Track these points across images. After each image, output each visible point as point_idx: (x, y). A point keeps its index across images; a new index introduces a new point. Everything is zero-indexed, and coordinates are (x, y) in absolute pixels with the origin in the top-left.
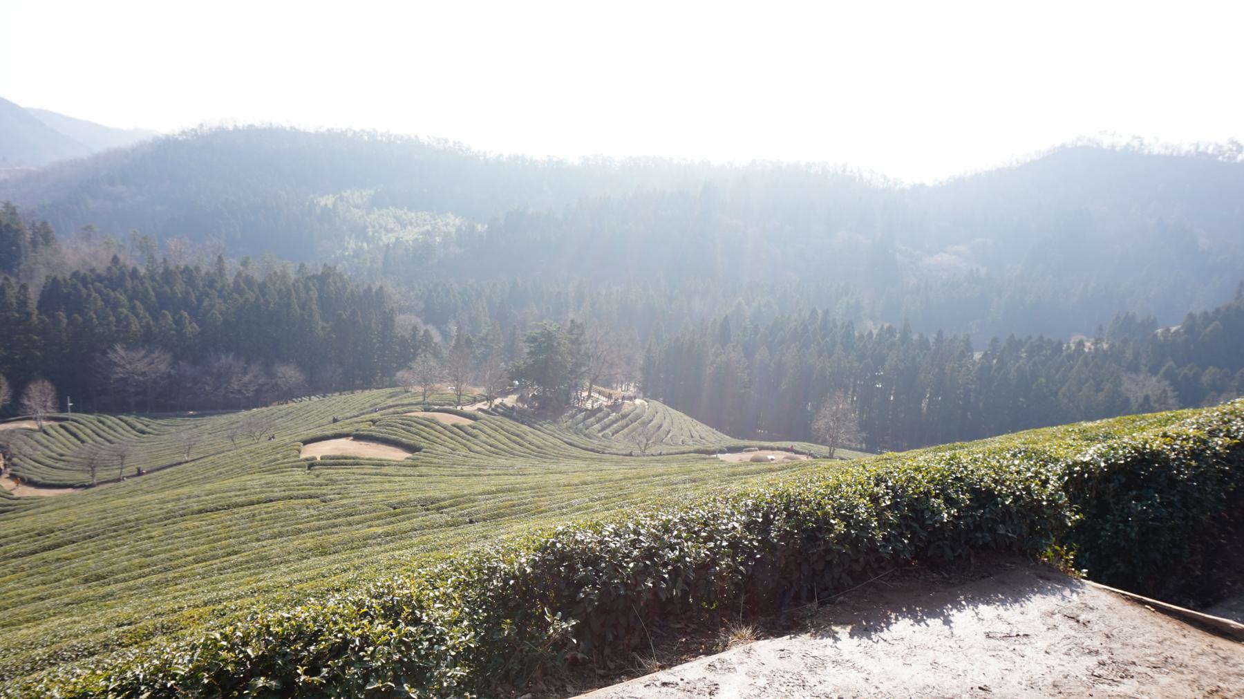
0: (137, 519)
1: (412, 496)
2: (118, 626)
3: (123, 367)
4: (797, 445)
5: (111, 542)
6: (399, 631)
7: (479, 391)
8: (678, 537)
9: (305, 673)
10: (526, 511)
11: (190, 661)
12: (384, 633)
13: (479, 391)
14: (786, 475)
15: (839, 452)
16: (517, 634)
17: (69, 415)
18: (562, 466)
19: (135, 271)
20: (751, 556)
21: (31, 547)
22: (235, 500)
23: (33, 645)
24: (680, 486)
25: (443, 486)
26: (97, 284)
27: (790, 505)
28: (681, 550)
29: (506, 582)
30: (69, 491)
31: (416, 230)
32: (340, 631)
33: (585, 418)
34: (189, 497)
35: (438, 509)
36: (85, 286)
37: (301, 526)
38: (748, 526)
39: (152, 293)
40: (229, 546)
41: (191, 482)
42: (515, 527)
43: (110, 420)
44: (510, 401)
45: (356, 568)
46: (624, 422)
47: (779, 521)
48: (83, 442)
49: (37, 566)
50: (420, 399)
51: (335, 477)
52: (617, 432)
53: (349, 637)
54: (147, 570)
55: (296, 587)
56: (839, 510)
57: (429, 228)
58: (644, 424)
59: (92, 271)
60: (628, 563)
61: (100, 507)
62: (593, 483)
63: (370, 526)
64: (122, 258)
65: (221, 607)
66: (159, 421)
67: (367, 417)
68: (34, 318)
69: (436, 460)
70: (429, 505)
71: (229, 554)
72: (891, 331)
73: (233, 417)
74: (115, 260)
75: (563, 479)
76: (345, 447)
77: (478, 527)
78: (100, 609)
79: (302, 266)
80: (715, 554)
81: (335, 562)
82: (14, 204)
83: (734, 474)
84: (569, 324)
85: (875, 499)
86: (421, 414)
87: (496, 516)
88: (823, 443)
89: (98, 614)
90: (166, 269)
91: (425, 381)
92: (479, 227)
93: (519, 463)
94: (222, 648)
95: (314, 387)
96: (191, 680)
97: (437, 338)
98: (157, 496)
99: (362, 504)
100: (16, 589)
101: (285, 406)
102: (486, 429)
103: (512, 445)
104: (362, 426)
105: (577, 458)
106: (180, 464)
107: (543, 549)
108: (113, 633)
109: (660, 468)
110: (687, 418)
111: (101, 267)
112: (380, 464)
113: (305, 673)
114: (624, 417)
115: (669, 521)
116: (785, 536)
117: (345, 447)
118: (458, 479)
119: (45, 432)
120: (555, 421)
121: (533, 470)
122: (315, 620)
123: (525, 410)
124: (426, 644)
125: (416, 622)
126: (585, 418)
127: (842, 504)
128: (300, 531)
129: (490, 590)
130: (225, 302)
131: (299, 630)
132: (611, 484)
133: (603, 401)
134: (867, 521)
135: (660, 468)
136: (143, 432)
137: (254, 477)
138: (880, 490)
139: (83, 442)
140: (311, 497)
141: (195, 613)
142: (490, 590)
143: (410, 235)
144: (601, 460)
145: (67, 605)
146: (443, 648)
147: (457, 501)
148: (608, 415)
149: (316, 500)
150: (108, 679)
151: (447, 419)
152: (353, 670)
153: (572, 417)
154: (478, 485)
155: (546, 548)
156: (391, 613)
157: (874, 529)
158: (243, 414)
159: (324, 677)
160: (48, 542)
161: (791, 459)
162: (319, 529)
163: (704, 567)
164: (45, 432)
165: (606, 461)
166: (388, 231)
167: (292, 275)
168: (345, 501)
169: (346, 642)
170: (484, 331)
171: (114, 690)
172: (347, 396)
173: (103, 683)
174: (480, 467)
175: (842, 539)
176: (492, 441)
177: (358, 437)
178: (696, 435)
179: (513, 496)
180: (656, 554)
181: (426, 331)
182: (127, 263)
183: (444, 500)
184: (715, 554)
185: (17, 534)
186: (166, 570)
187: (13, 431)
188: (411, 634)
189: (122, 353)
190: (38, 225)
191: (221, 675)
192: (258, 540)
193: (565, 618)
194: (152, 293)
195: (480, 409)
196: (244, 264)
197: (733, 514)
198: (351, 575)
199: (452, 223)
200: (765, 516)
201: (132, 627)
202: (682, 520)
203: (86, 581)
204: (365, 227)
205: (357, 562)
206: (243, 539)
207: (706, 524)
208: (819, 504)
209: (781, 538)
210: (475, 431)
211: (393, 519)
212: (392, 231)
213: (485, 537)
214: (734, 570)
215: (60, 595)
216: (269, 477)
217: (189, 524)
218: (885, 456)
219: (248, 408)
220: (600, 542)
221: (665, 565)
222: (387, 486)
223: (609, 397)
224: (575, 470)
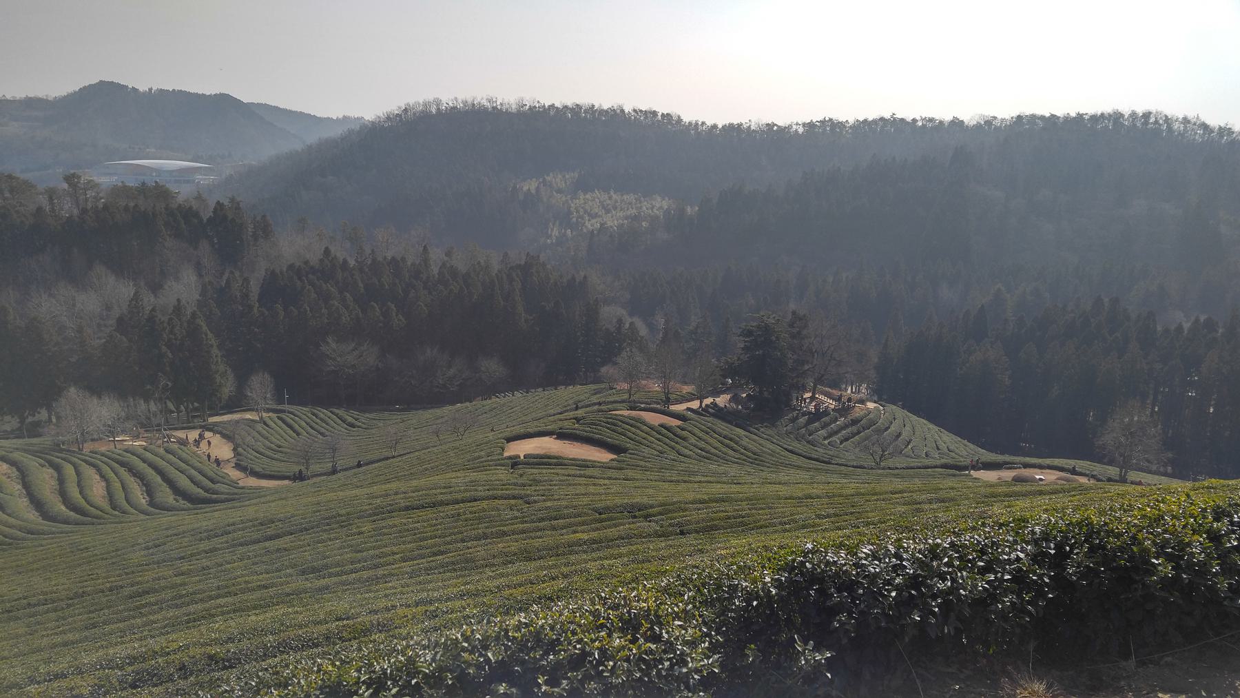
0: (348, 514)
1: (618, 501)
2: (338, 620)
3: (334, 359)
4: (1081, 464)
5: (325, 536)
6: (639, 648)
7: (687, 389)
8: (948, 565)
9: (546, 683)
10: (743, 524)
11: (433, 660)
12: (623, 648)
13: (687, 389)
14: (1061, 500)
15: (1133, 475)
16: (761, 662)
17: (286, 407)
18: (782, 477)
19: (345, 261)
20: (1041, 594)
21: (255, 536)
22: (440, 498)
23: (264, 632)
24: (926, 507)
25: (651, 491)
26: (310, 276)
27: (1092, 535)
28: (954, 580)
29: (748, 601)
30: (286, 482)
31: (621, 214)
32: (580, 641)
33: (810, 422)
34: (396, 494)
35: (646, 517)
36: (300, 279)
37: (505, 529)
38: (1038, 558)
39: (361, 285)
40: (435, 545)
41: (398, 478)
42: (734, 542)
43: (323, 413)
44: (722, 400)
45: (565, 576)
46: (854, 429)
47: (1078, 555)
48: (298, 434)
49: (261, 555)
50: (626, 396)
51: (538, 477)
52: (846, 440)
53: (588, 649)
54: (358, 565)
55: (507, 592)
56: (1163, 547)
57: (634, 211)
58: (880, 431)
59: (306, 263)
60: (889, 591)
61: (314, 500)
62: (818, 497)
63: (575, 532)
64: (333, 249)
65: (432, 608)
66: (367, 415)
67: (571, 414)
68: (255, 310)
69: (642, 463)
70: (636, 511)
71: (435, 554)
72: (1210, 325)
73: (438, 412)
74: (327, 251)
75: (784, 491)
76: (548, 445)
77: (690, 539)
78: (318, 601)
79: (506, 255)
80: (995, 588)
81: (542, 568)
82: (239, 199)
83: (993, 495)
84: (790, 316)
85: (1215, 537)
86: (626, 413)
87: (709, 529)
88: (1110, 463)
89: (316, 606)
90: (374, 260)
91: (631, 377)
92: (689, 209)
93: (733, 470)
94: (464, 650)
95: (517, 381)
96: (434, 680)
97: (643, 331)
98: (366, 491)
99: (567, 507)
100: (243, 576)
101: (489, 401)
102: (697, 431)
103: (724, 449)
104: (566, 424)
105: (799, 467)
106: (387, 458)
107: (790, 568)
108: (334, 626)
109: (899, 484)
110: (931, 426)
111: (314, 257)
112: (584, 464)
113: (546, 683)
114: (855, 422)
115: (938, 545)
116: (1089, 573)
117: (548, 445)
118: (666, 485)
119: (265, 423)
120: (773, 425)
121: (749, 479)
122: (552, 628)
123: (740, 411)
124: (667, 664)
125: (656, 639)
126: (810, 422)
127: (1167, 541)
128: (504, 534)
129: (732, 610)
130: (430, 293)
131: (538, 636)
132: (841, 500)
133: (832, 404)
134: (1204, 565)
135: (899, 484)
136: (352, 426)
137: (459, 474)
138: (1222, 526)
139: (298, 434)
140: (514, 498)
141: (409, 612)
142: (732, 610)
143: (613, 221)
144: (827, 471)
145: (288, 595)
146: (685, 670)
147: (667, 509)
148: (836, 420)
149: (520, 501)
150: (359, 671)
151: (654, 419)
152: (593, 685)
153: (794, 420)
154: (686, 493)
155: (794, 568)
156: (630, 626)
157: (1216, 574)
158: (447, 410)
159: (564, 689)
160: (270, 532)
161: (1067, 480)
162: (523, 532)
163: (984, 602)
164: (265, 423)
165: (833, 472)
166: (593, 216)
167: (496, 266)
168: (549, 504)
169: (585, 654)
170: (694, 324)
171: (364, 682)
172: (550, 392)
173: (355, 674)
174: (694, 473)
175: (1167, 583)
176: (702, 445)
177: (562, 436)
178: (943, 446)
179: (726, 506)
180: (923, 583)
181: (631, 324)
182: (338, 255)
183: (652, 507)
184: (995, 588)
185: (242, 522)
186: (376, 567)
187: (237, 422)
188: (651, 652)
189: (334, 345)
190: (259, 218)
191: (462, 678)
192: (463, 541)
193: (817, 649)
194: (361, 285)
195: (689, 409)
196: (448, 254)
197: (1015, 542)
198: (562, 584)
199: (660, 205)
200: (1059, 547)
201: (351, 622)
202: (952, 544)
203: (303, 572)
204: (569, 213)
205: (565, 570)
206: (448, 539)
207: (983, 552)
208: (1134, 538)
209: (1082, 576)
210: (685, 433)
211: (598, 525)
212: (596, 216)
213: (701, 551)
214: (1018, 609)
215: (281, 585)
216: (474, 475)
217: (397, 521)
218: (1206, 484)
219: (453, 403)
220: (856, 565)
221: (934, 597)
222: (592, 489)
223: (839, 399)
224: (794, 481)
